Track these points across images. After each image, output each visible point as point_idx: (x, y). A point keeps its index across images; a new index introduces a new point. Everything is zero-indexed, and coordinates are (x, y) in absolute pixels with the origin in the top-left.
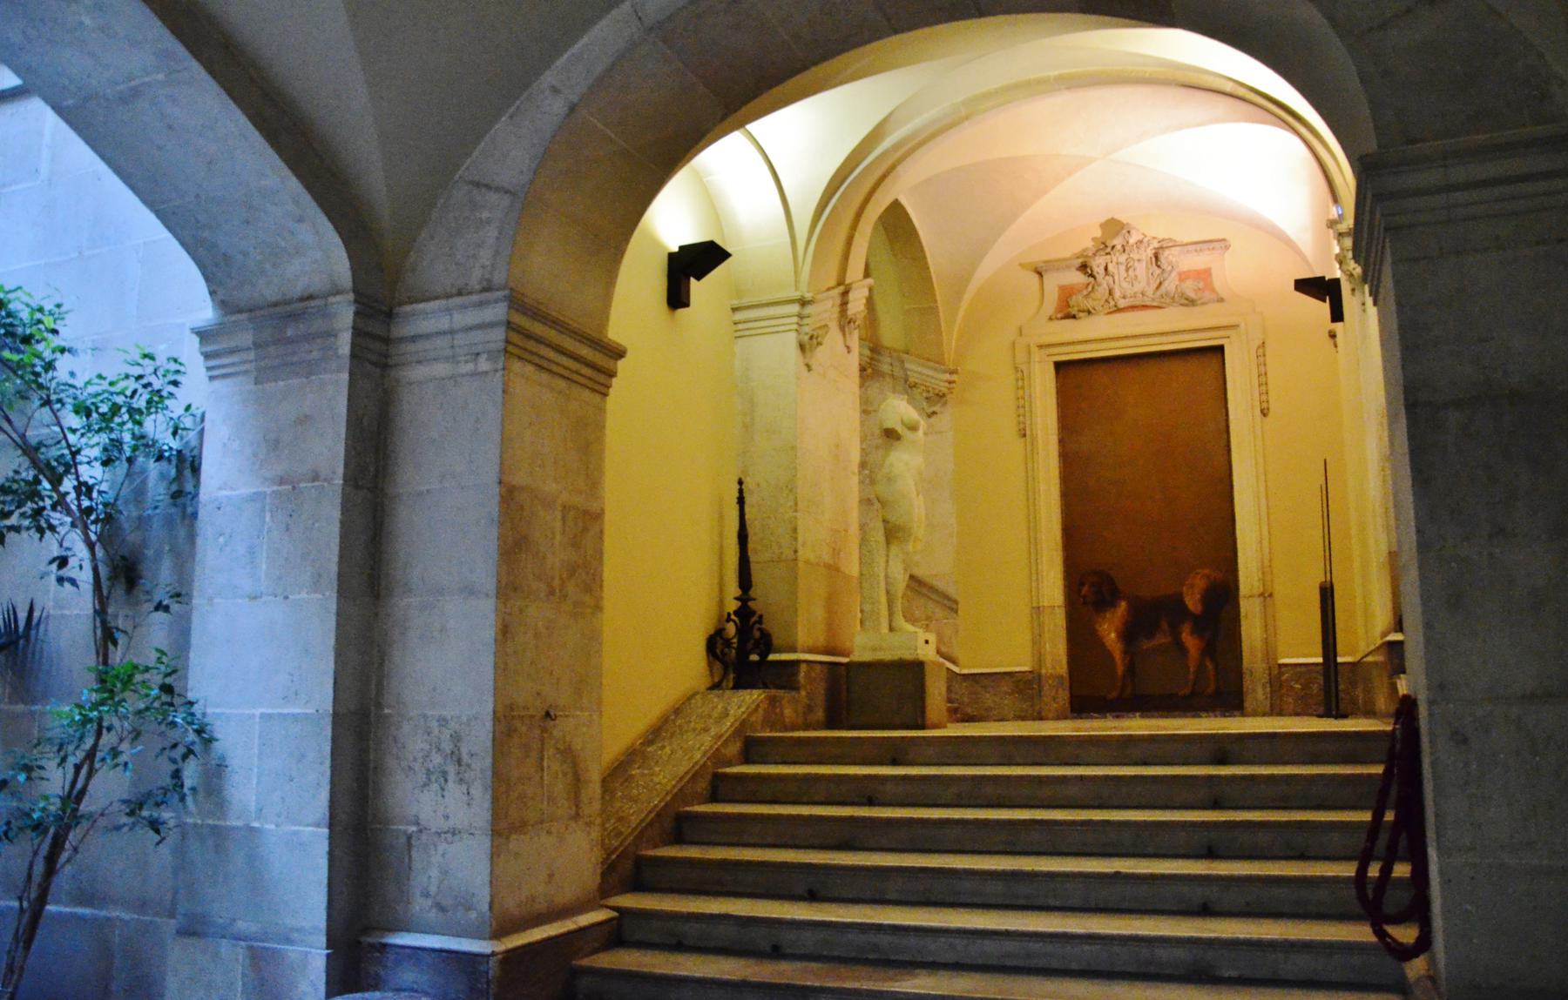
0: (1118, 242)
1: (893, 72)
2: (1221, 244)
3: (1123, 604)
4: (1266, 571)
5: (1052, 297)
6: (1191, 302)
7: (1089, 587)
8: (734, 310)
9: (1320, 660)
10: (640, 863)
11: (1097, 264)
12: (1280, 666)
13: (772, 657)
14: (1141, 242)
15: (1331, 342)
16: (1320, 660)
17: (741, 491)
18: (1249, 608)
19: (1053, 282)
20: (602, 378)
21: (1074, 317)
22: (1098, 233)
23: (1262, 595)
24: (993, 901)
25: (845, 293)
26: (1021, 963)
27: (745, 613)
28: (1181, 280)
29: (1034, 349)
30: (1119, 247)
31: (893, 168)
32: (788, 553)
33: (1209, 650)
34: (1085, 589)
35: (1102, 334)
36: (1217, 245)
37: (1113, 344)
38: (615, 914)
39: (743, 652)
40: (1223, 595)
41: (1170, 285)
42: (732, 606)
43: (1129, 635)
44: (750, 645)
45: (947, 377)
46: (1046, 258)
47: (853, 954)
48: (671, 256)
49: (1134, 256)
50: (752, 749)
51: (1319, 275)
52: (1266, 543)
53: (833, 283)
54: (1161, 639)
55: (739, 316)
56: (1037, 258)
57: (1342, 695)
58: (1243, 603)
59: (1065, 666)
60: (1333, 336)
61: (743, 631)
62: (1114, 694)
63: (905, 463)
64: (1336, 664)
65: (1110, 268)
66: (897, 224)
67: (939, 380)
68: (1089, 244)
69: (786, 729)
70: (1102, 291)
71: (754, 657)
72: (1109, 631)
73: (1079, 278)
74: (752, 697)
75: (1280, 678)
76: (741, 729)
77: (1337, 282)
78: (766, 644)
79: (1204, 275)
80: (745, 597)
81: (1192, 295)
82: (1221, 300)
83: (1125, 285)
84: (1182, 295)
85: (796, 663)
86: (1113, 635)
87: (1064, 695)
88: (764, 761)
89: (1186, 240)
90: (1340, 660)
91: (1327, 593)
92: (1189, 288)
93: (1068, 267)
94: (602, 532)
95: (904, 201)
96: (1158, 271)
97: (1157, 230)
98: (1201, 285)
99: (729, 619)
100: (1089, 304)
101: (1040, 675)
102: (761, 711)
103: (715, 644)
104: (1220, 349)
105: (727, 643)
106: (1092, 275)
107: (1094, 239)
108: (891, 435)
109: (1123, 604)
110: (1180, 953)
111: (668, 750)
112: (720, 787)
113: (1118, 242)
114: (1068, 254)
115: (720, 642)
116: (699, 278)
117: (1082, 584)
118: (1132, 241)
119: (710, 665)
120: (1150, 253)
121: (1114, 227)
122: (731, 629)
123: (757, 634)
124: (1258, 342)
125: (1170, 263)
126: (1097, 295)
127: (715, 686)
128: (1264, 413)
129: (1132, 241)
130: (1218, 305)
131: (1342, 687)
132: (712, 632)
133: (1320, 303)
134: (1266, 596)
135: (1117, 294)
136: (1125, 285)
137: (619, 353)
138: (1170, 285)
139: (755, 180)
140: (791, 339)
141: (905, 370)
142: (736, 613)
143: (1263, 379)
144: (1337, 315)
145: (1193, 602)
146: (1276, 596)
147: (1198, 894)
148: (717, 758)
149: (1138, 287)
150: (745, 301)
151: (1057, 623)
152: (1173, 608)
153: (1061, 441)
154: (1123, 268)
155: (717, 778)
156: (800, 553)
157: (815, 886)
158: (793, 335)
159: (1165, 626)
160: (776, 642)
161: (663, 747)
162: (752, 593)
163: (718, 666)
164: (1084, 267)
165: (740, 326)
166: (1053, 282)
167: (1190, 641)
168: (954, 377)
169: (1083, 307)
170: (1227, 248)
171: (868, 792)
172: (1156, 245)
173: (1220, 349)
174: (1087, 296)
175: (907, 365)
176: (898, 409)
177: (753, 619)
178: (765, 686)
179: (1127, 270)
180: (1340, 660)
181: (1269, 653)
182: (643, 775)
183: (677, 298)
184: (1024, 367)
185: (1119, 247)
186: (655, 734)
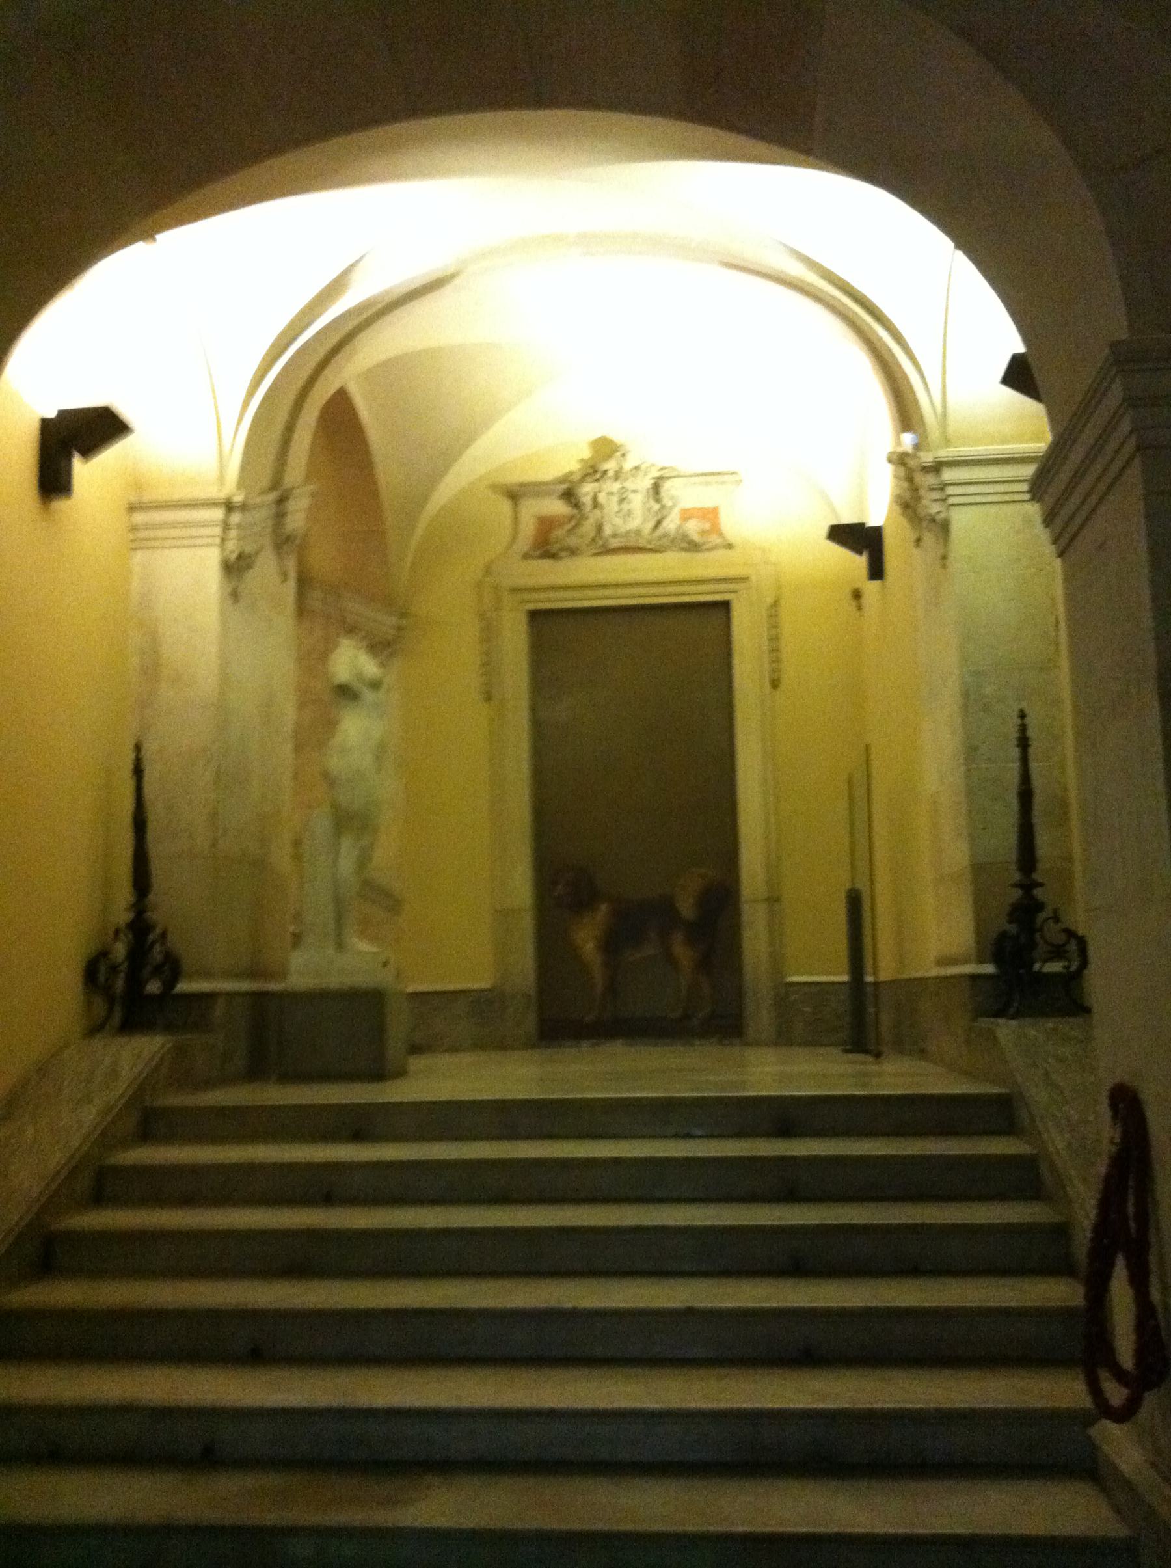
0: (610, 466)
1: (372, 179)
3: (604, 908)
4: (773, 868)
5: (528, 528)
7: (564, 884)
8: (132, 508)
9: (845, 978)
11: (587, 490)
13: (183, 987)
14: (637, 468)
16: (845, 978)
19: (533, 509)
23: (768, 900)
25: (282, 500)
27: (140, 927)
30: (611, 473)
33: (705, 964)
34: (560, 889)
37: (661, 590)
39: (135, 981)
41: (671, 524)
42: (122, 916)
43: (611, 945)
45: (394, 620)
48: (45, 423)
49: (629, 485)
50: (150, 1123)
54: (650, 950)
55: (139, 518)
56: (516, 477)
63: (355, 729)
66: (340, 421)
67: (386, 622)
70: (588, 528)
71: (153, 987)
72: (587, 938)
73: (558, 508)
74: (148, 1047)
75: (786, 998)
77: (877, 532)
78: (172, 968)
79: (710, 515)
81: (696, 538)
82: (730, 546)
84: (685, 537)
85: (211, 996)
87: (531, 1022)
88: (169, 1138)
91: (854, 902)
92: (693, 528)
93: (548, 494)
96: (657, 507)
98: (707, 526)
100: (572, 541)
103: (94, 972)
104: (725, 606)
106: (577, 505)
108: (346, 693)
109: (604, 908)
113: (610, 466)
115: (103, 969)
119: (89, 1004)
120: (647, 483)
122: (120, 951)
125: (672, 498)
128: (775, 684)
130: (727, 552)
133: (856, 557)
134: (773, 900)
136: (618, 521)
138: (671, 524)
144: (876, 571)
145: (687, 908)
149: (634, 523)
150: (146, 498)
152: (662, 912)
153: (533, 709)
154: (615, 499)
157: (258, 1343)
166: (533, 509)
167: (683, 953)
171: (323, 1186)
172: (658, 474)
173: (725, 606)
174: (571, 531)
176: (350, 661)
178: (169, 1028)
179: (622, 500)
181: (777, 962)
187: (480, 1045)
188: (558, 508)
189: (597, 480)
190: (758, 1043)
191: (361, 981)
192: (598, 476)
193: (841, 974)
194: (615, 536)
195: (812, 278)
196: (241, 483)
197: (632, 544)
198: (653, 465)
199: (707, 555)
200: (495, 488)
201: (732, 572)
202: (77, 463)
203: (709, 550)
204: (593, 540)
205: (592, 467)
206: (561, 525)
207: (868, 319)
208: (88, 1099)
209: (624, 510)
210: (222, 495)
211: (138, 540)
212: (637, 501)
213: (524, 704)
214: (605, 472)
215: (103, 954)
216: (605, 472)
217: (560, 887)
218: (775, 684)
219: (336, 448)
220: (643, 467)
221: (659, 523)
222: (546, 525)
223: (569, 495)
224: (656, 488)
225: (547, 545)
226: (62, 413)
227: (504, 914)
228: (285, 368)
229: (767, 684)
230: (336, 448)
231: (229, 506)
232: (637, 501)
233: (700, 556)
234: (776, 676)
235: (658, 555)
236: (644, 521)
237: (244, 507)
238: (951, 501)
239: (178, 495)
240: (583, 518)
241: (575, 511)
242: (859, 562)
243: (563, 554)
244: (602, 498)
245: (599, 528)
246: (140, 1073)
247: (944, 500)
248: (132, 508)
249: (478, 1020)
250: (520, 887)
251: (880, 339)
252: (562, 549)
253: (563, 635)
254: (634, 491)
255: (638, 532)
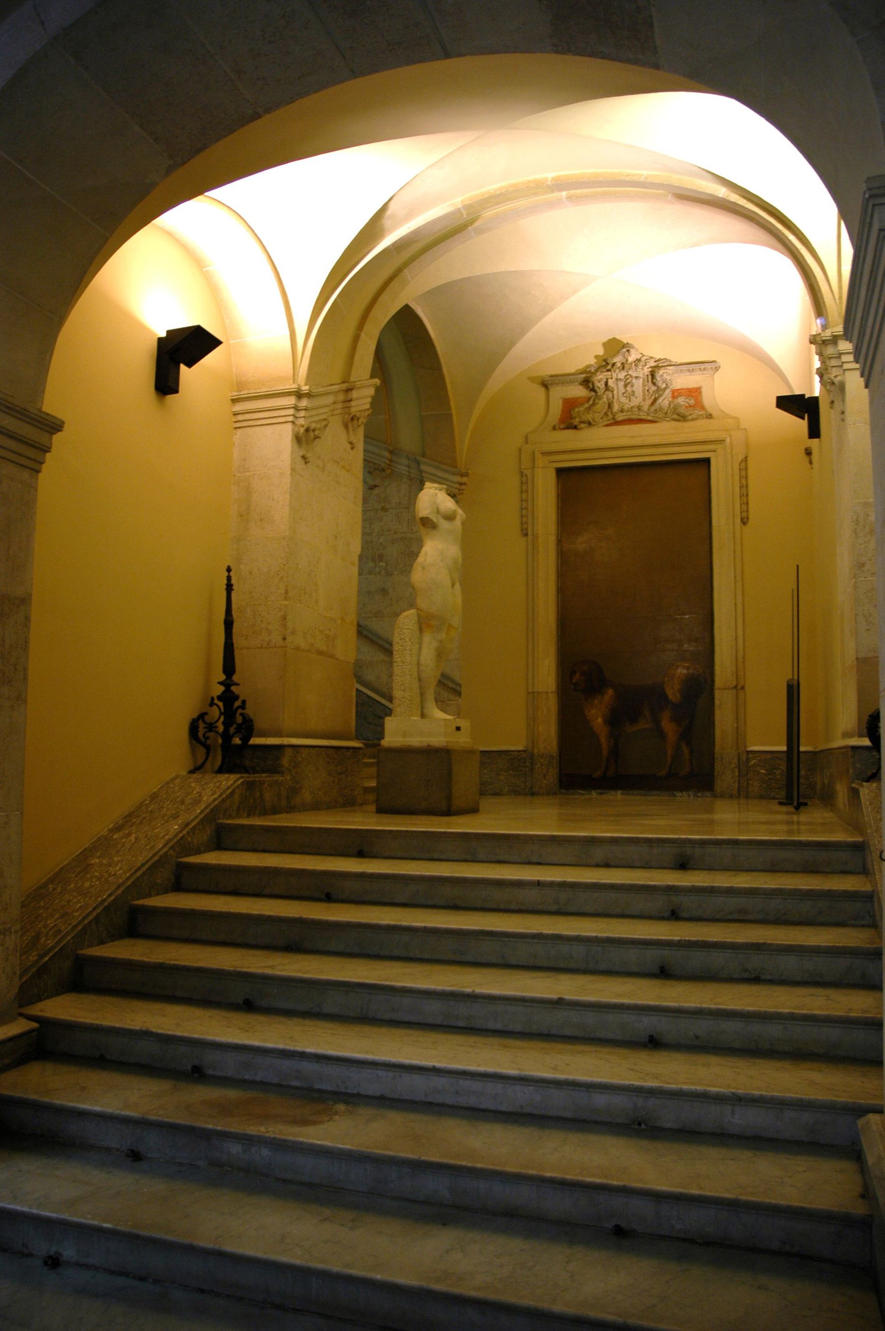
0: (618, 360)
2: (709, 366)
3: (611, 692)
5: (556, 408)
6: (683, 418)
7: (582, 673)
8: (234, 401)
9: (784, 748)
10: (81, 963)
11: (599, 379)
12: (748, 752)
13: (255, 741)
14: (639, 360)
15: (806, 459)
16: (784, 748)
17: (229, 578)
18: (723, 700)
19: (559, 394)
20: (30, 452)
21: (575, 428)
22: (601, 352)
23: (736, 687)
24: (430, 1021)
26: (450, 1101)
27: (228, 698)
28: (674, 397)
29: (538, 455)
31: (399, 271)
32: (276, 638)
35: (603, 443)
36: (708, 366)
38: (35, 1025)
39: (227, 737)
40: (700, 688)
43: (614, 720)
44: (232, 730)
45: (457, 479)
46: (552, 373)
47: (275, 1080)
48: (160, 339)
51: (797, 392)
52: (740, 641)
53: (338, 380)
55: (238, 407)
57: (801, 781)
58: (717, 694)
59: (555, 743)
60: (808, 452)
61: (229, 714)
62: (598, 774)
64: (798, 751)
65: (610, 383)
68: (593, 361)
69: (264, 813)
71: (237, 741)
72: (597, 715)
73: (580, 392)
74: (229, 781)
75: (747, 762)
76: (212, 816)
77: (815, 400)
78: (248, 728)
80: (228, 684)
81: (682, 410)
82: (710, 416)
83: (623, 400)
85: (280, 748)
86: (600, 720)
87: (553, 775)
88: (234, 848)
89: (679, 361)
90: (802, 749)
91: (793, 692)
93: (571, 382)
94: (27, 618)
95: (413, 306)
96: (654, 388)
97: (657, 352)
98: (692, 402)
99: (212, 704)
100: (589, 417)
101: (533, 754)
102: (237, 797)
103: (197, 729)
104: (707, 462)
105: (211, 727)
106: (593, 390)
107: (596, 357)
109: (611, 692)
110: (620, 1101)
111: (133, 838)
112: (183, 879)
113: (618, 360)
114: (572, 370)
115: (201, 725)
116: (189, 365)
117: (575, 673)
118: (631, 359)
120: (647, 370)
121: (615, 346)
123: (239, 719)
124: (741, 457)
126: (598, 407)
127: (196, 769)
128: (744, 521)
129: (631, 359)
130: (708, 421)
131: (802, 773)
132: (195, 716)
134: (739, 688)
135: (616, 408)
136: (623, 400)
137: (54, 426)
138: (665, 401)
139: (241, 261)
140: (287, 431)
141: (421, 471)
142: (220, 698)
143: (744, 499)
144: (814, 432)
145: (673, 693)
146: (747, 687)
147: (646, 1024)
148: (183, 846)
149: (635, 402)
150: (244, 393)
151: (550, 707)
153: (559, 542)
154: (621, 384)
155: (182, 868)
156: (289, 639)
158: (289, 426)
159: (647, 713)
160: (258, 724)
161: (129, 834)
162: (235, 678)
163: (201, 751)
164: (587, 383)
165: (240, 418)
166: (559, 394)
167: (669, 727)
168: (465, 480)
169: (584, 418)
170: (717, 369)
171: (326, 889)
172: (653, 364)
173: (707, 462)
174: (589, 408)
175: (423, 467)
177: (237, 704)
179: (626, 386)
180: (802, 749)
181: (739, 736)
182: (101, 864)
183: (166, 383)
184: (528, 472)
185: (619, 365)
186: (128, 821)
187: (516, 792)
188: (580, 392)
189: (609, 370)
190: (722, 796)
191: (438, 741)
192: (609, 367)
193: (781, 745)
194: (622, 411)
195: (735, 198)
196: (309, 379)
197: (634, 417)
198: (651, 358)
199: (691, 423)
200: (532, 379)
201: (712, 436)
202: (183, 368)
203: (693, 420)
204: (606, 414)
205: (605, 360)
206: (582, 404)
207: (779, 226)
208: (175, 817)
209: (627, 390)
210: (293, 387)
211: (240, 422)
212: (638, 386)
213: (552, 539)
214: (614, 364)
215: (202, 716)
216: (614, 364)
217: (578, 675)
218: (744, 521)
219: (404, 355)
220: (643, 359)
221: (655, 400)
222: (570, 404)
223: (587, 383)
224: (653, 374)
225: (569, 419)
226: (169, 332)
227: (533, 696)
228: (339, 296)
229: (738, 521)
230: (404, 355)
231: (299, 395)
232: (638, 386)
233: (686, 424)
234: (744, 514)
235: (653, 425)
236: (644, 400)
237: (309, 395)
238: (846, 366)
239: (264, 390)
240: (598, 397)
241: (593, 394)
242: (801, 425)
243: (583, 425)
244: (611, 383)
245: (610, 406)
246: (215, 800)
247: (841, 366)
248: (234, 401)
249: (510, 774)
250: (547, 674)
251: (790, 241)
252: (582, 422)
253: (583, 487)
254: (636, 378)
255: (639, 408)
